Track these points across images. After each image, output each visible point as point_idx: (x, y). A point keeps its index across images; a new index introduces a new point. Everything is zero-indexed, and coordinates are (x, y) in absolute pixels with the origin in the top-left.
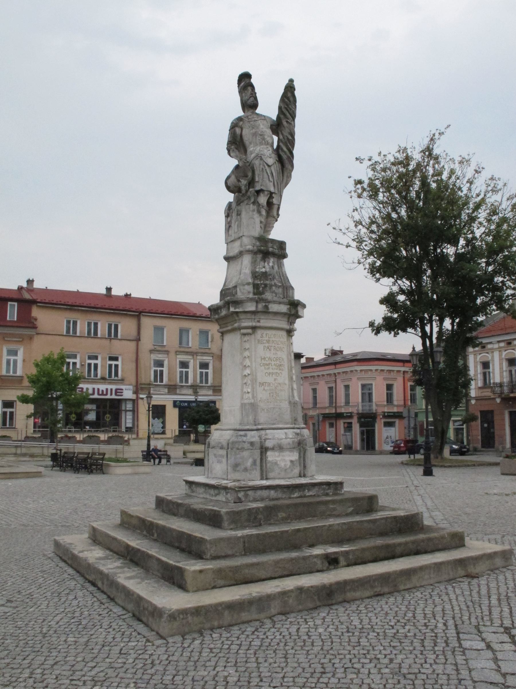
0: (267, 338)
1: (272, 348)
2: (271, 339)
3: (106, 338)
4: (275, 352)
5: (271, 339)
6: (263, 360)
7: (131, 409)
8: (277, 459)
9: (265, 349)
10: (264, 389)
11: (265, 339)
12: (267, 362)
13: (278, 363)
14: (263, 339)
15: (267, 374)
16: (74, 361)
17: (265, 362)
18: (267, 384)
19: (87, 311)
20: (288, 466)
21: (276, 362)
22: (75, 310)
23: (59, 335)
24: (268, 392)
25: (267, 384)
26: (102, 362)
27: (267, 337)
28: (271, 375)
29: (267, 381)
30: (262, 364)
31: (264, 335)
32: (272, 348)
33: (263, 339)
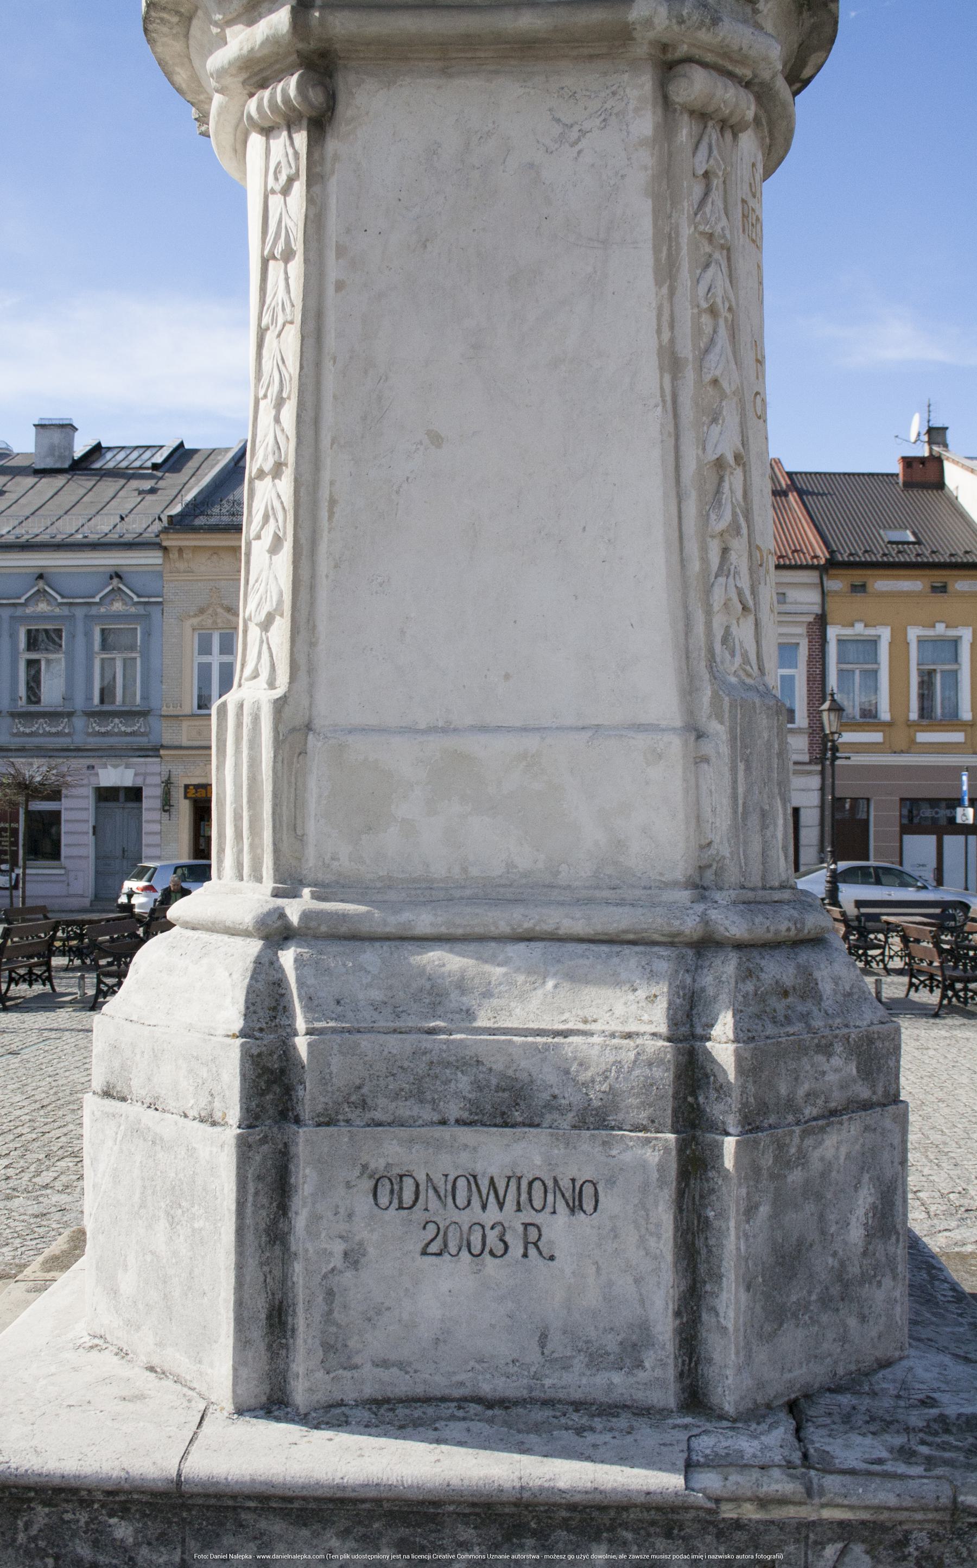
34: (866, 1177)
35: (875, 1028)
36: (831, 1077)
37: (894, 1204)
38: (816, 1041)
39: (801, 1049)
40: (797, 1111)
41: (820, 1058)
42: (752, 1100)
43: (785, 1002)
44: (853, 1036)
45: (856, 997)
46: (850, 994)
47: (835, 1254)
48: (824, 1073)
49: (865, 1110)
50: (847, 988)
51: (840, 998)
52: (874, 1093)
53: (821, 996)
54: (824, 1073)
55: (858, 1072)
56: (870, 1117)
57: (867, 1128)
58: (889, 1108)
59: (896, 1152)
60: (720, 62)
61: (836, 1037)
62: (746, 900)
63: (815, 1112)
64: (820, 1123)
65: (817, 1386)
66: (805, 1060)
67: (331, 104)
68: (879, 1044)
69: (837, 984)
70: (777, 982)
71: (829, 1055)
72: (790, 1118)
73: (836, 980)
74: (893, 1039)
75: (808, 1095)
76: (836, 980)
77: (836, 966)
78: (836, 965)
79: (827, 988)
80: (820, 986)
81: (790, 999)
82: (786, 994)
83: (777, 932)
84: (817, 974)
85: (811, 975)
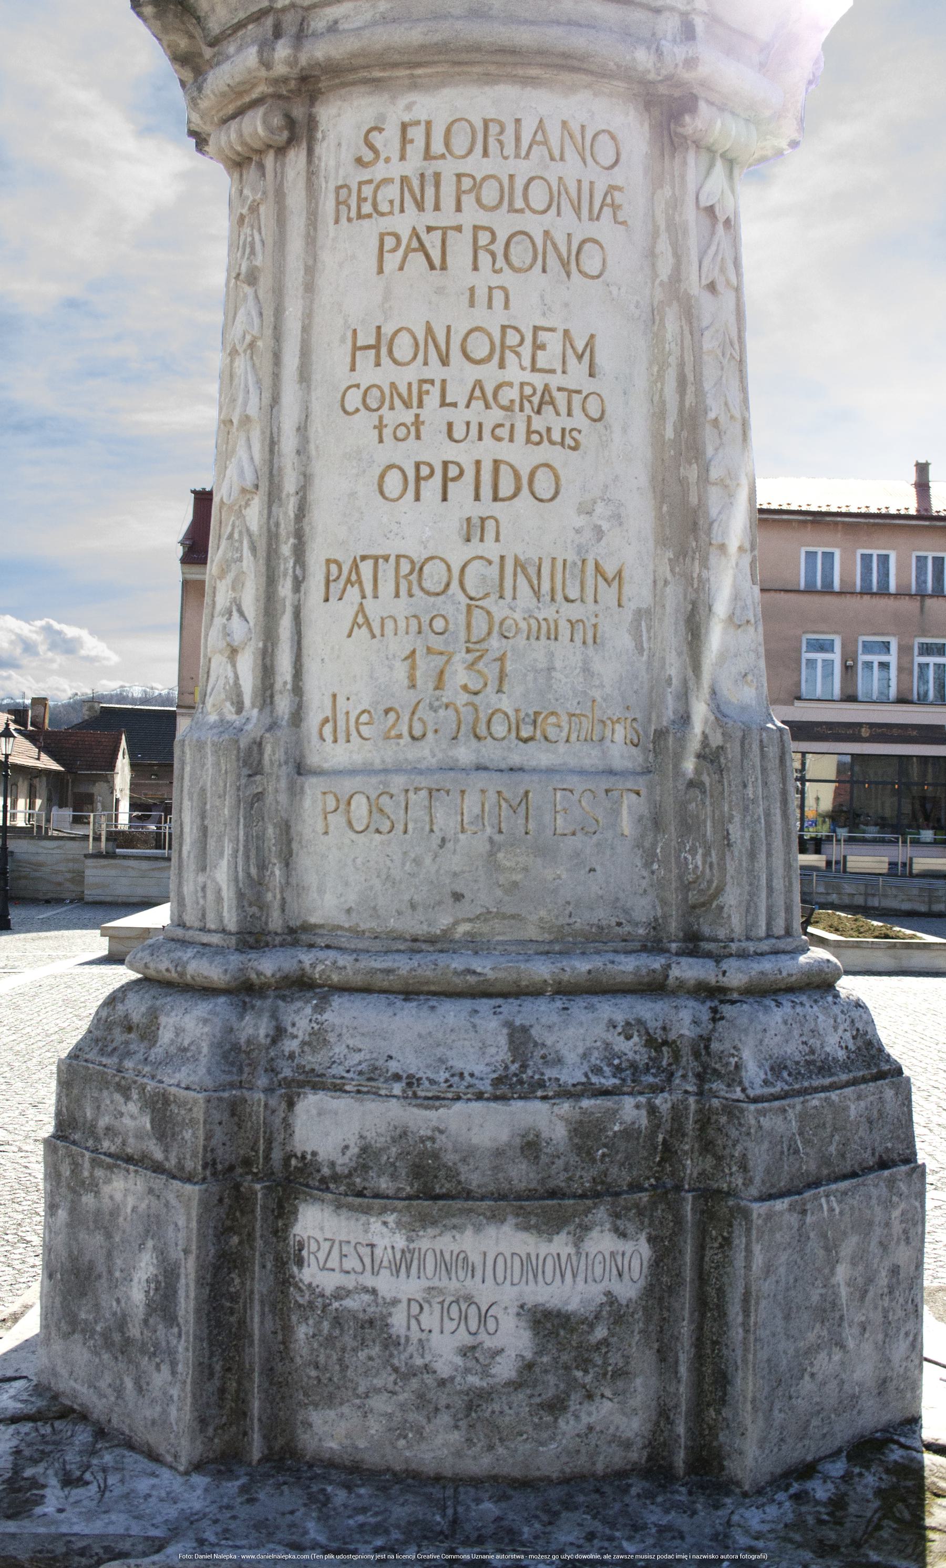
0: (413, 165)
1: (460, 248)
2: (448, 168)
3: (910, 595)
4: (484, 278)
5: (448, 168)
6: (366, 359)
7: (807, 784)
8: (385, 1284)
9: (392, 261)
10: (361, 619)
11: (396, 170)
12: (407, 376)
13: (514, 372)
14: (380, 171)
15: (393, 482)
16: (884, 658)
17: (386, 374)
18: (387, 572)
19: (874, 525)
20: (505, 1369)
21: (490, 374)
22: (828, 524)
23: (776, 590)
24: (399, 645)
25: (387, 572)
26: (899, 658)
27: (415, 151)
28: (432, 488)
29: (393, 547)
30: (354, 399)
31: (388, 141)
32: (460, 248)
33: (380, 171)
34: (150, 1244)
35: (173, 1090)
36: (127, 1121)
37: (176, 1292)
38: (117, 1079)
39: (104, 1083)
40: (97, 1139)
41: (118, 1097)
42: (64, 1110)
43: (126, 1036)
44: (149, 1088)
45: (189, 1054)
46: (185, 1050)
47: (118, 1301)
48: (122, 1114)
49: (154, 1172)
50: (186, 1044)
51: (173, 1050)
52: (167, 1159)
53: (156, 1042)
54: (122, 1114)
55: (153, 1128)
56: (159, 1181)
57: (151, 1191)
58: (175, 1182)
59: (180, 1235)
60: (239, 103)
61: (135, 1082)
62: (175, 936)
63: (113, 1149)
64: (108, 1160)
65: (95, 1416)
66: (105, 1093)
67: (310, 263)
68: (173, 1106)
69: (177, 1035)
70: (126, 1016)
71: (128, 1098)
72: (90, 1143)
73: (179, 1031)
74: (191, 1110)
75: (108, 1129)
76: (179, 1031)
77: (187, 1018)
78: (187, 1017)
79: (166, 1036)
80: (160, 1032)
81: (132, 1036)
82: (130, 1029)
83: (158, 972)
84: (163, 1020)
85: (156, 1018)
